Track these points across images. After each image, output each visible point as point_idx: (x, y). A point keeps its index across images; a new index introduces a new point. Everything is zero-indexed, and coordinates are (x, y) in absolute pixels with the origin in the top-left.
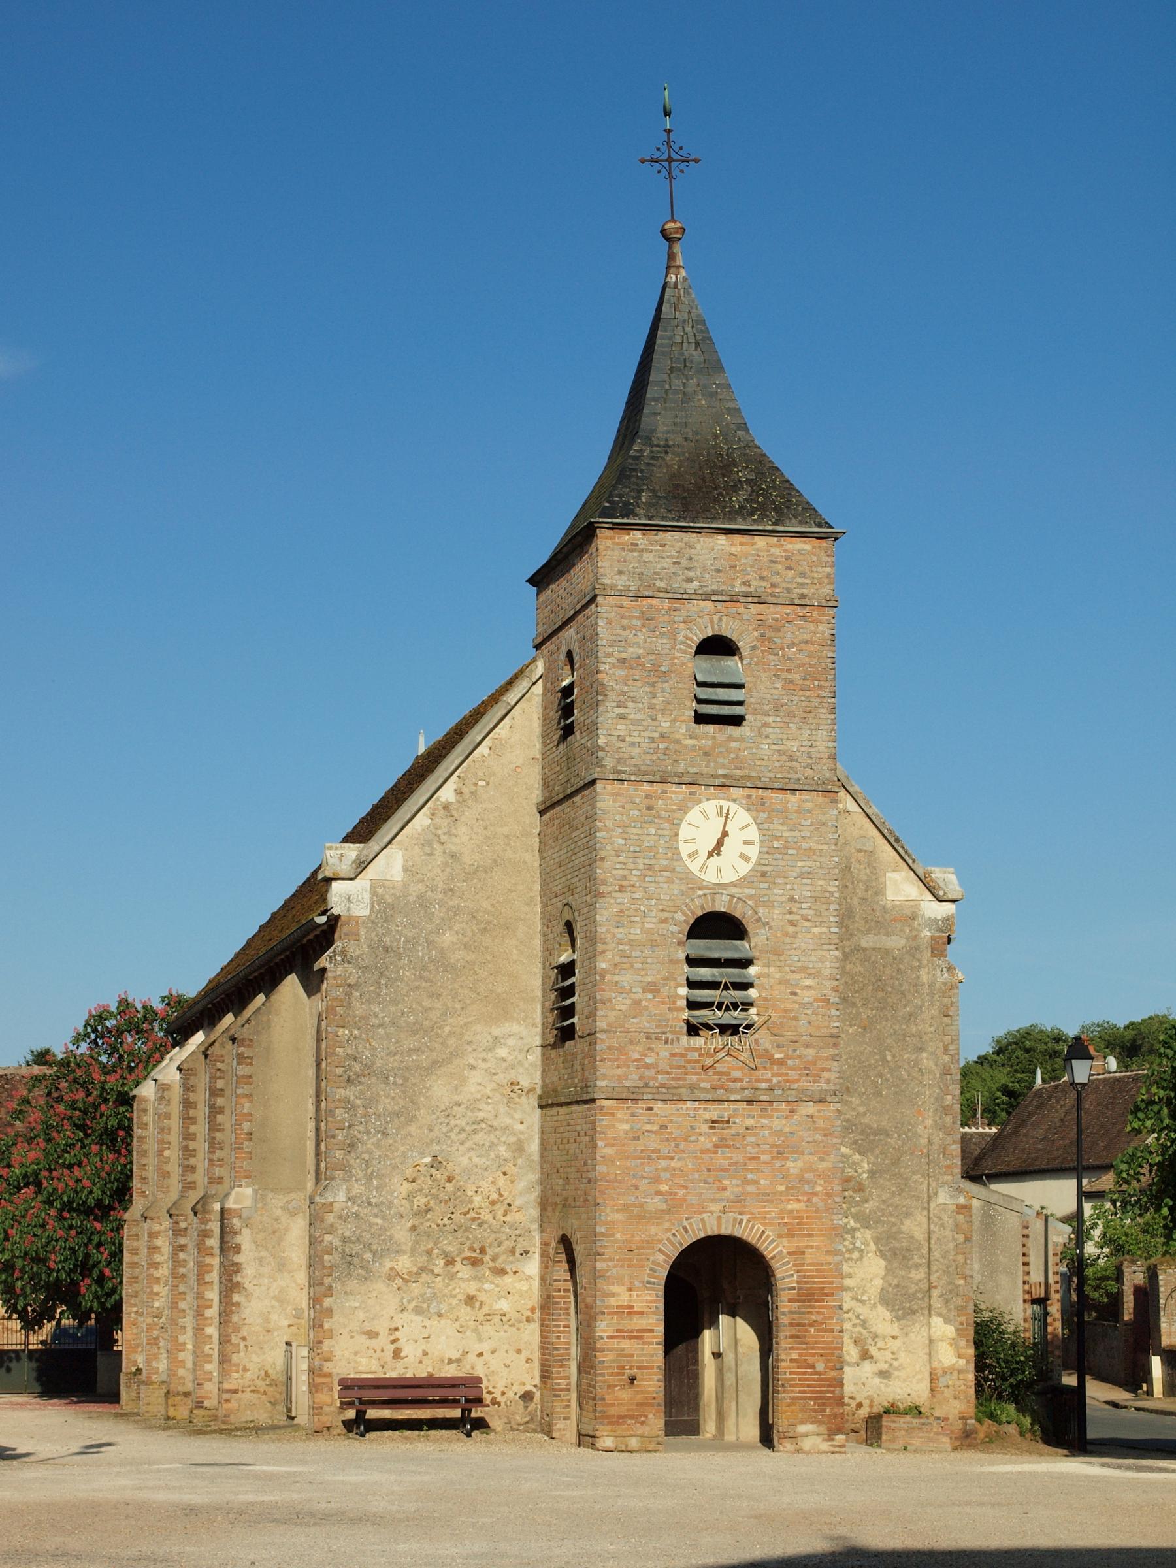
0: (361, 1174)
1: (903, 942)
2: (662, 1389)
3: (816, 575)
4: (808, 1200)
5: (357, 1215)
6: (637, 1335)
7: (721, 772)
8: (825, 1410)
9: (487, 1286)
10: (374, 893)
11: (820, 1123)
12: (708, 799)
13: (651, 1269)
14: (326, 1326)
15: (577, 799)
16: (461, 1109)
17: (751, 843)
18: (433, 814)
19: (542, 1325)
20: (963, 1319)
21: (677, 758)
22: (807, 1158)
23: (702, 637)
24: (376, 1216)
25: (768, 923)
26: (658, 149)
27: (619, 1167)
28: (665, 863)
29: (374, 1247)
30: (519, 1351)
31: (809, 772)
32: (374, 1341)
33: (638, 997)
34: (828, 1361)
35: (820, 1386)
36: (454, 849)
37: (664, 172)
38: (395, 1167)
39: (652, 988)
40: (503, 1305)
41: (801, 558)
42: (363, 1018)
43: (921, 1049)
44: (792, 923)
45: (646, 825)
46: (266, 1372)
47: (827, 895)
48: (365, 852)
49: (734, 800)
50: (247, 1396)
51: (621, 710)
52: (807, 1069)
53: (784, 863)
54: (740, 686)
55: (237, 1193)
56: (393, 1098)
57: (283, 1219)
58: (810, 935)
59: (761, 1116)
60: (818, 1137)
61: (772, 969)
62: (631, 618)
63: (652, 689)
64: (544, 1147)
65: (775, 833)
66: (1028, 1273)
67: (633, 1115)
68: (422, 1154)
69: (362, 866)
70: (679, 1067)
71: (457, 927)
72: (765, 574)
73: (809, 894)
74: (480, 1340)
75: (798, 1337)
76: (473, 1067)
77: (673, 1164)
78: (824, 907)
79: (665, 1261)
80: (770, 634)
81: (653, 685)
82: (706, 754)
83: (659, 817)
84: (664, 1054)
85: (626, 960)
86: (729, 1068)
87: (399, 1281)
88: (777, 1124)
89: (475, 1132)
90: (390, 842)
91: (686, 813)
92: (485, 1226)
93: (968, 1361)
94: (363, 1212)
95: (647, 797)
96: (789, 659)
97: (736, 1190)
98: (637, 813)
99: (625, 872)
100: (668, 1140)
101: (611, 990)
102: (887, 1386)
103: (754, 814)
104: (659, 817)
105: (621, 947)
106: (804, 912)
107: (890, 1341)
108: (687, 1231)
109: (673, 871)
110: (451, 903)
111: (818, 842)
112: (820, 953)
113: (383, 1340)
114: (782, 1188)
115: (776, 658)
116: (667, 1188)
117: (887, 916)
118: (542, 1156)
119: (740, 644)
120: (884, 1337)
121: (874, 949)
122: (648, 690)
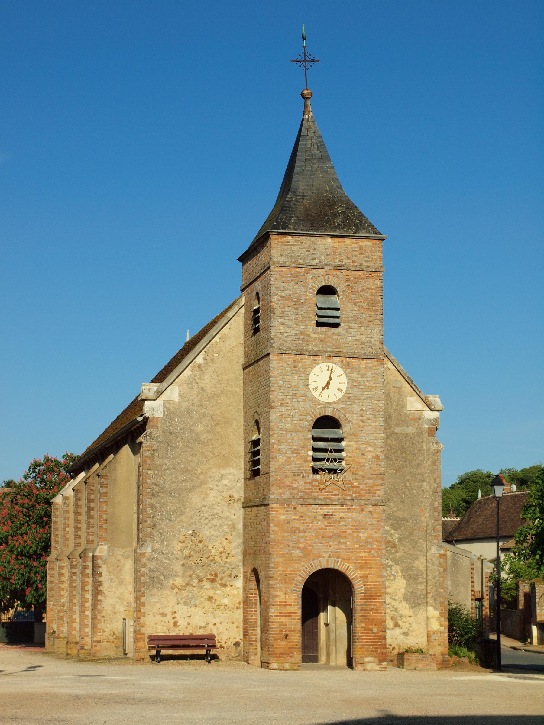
0: (159, 539)
1: (415, 430)
2: (301, 641)
3: (374, 257)
4: (370, 552)
6: (289, 615)
7: (329, 350)
8: (377, 651)
9: (218, 592)
10: (165, 407)
11: (375, 515)
12: (323, 363)
13: (295, 584)
15: (261, 362)
16: (206, 509)
17: (343, 383)
20: (443, 608)
21: (308, 343)
24: (166, 559)
25: (351, 421)
28: (303, 393)
29: (165, 573)
30: (233, 623)
31: (370, 350)
32: (164, 618)
33: (289, 456)
34: (379, 627)
35: (375, 639)
36: (203, 386)
37: (303, 67)
38: (174, 536)
39: (296, 452)
40: (226, 601)
41: (367, 249)
42: (160, 465)
43: (423, 481)
44: (362, 421)
46: (114, 633)
47: (379, 408)
49: (335, 363)
51: (281, 320)
53: (359, 393)
54: (338, 309)
55: (100, 548)
56: (174, 503)
58: (370, 427)
60: (374, 522)
61: (353, 443)
62: (286, 277)
63: (296, 311)
64: (245, 526)
65: (354, 379)
66: (474, 586)
68: (188, 530)
70: (309, 489)
71: (204, 423)
72: (350, 256)
73: (370, 407)
74: (215, 617)
75: (365, 616)
76: (211, 489)
77: (306, 534)
78: (378, 413)
79: (302, 580)
81: (297, 309)
83: (299, 371)
84: (302, 483)
86: (332, 489)
87: (176, 590)
88: (355, 516)
89: (212, 519)
90: (172, 383)
91: (312, 369)
92: (217, 564)
93: (445, 628)
94: (160, 557)
95: (294, 361)
96: (361, 296)
98: (289, 369)
99: (283, 397)
100: (303, 523)
101: (277, 453)
102: (407, 639)
103: (345, 369)
104: (299, 371)
105: (281, 432)
106: (368, 416)
107: (408, 618)
108: (312, 566)
110: (201, 411)
111: (374, 383)
112: (375, 435)
113: (169, 617)
114: (357, 546)
115: (355, 296)
116: (303, 546)
117: (407, 418)
119: (338, 289)
120: (405, 616)
121: (401, 433)
122: (294, 311)
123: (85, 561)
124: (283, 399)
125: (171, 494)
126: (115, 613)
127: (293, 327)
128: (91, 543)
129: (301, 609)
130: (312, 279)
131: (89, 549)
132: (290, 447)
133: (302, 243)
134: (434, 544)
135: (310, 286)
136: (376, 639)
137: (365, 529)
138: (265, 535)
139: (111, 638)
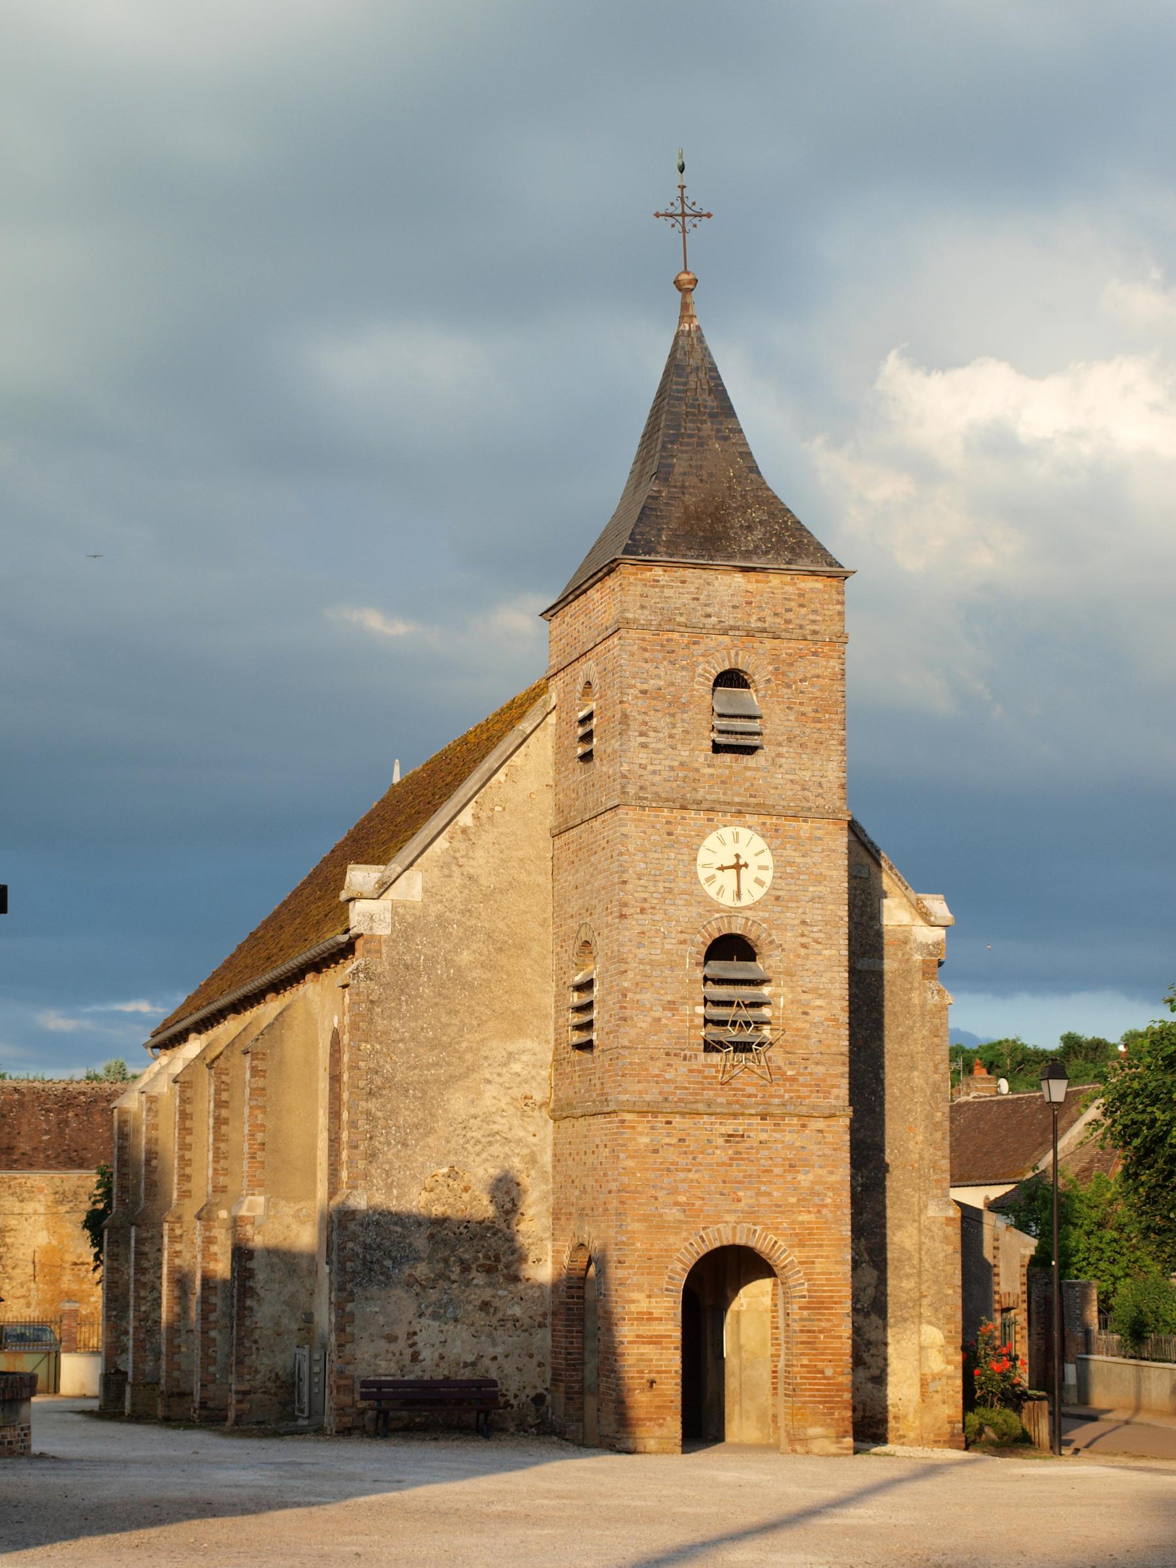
2: (679, 1393)
3: (827, 612)
4: (819, 1212)
5: (378, 1223)
6: (655, 1340)
7: (737, 799)
8: (833, 1414)
9: (500, 1292)
10: (394, 912)
11: (830, 1138)
13: (670, 1277)
14: (348, 1329)
15: (596, 824)
16: (477, 1122)
17: (766, 868)
18: (452, 838)
19: (554, 1330)
20: (952, 1327)
22: (820, 1172)
23: (720, 670)
26: (672, 204)
27: (640, 1179)
29: (394, 1254)
30: (531, 1356)
31: (820, 801)
32: (393, 1345)
33: (657, 1015)
34: (837, 1366)
35: (829, 1390)
36: (472, 871)
37: (678, 227)
39: (671, 1006)
40: (517, 1311)
41: (814, 595)
43: (913, 1068)
44: (804, 946)
45: (666, 850)
46: (277, 1374)
48: (387, 873)
49: (750, 827)
50: (259, 1396)
51: (643, 739)
52: (818, 1085)
53: (797, 888)
55: (251, 1201)
56: (413, 1111)
57: (294, 1227)
58: (820, 958)
59: (774, 1131)
60: (828, 1151)
62: (653, 650)
64: (557, 1158)
65: (789, 859)
67: (653, 1128)
68: (440, 1164)
69: (384, 887)
70: (697, 1083)
71: (475, 946)
72: (779, 611)
73: (820, 918)
74: (494, 1344)
75: (808, 1343)
76: (489, 1082)
77: (690, 1175)
78: (834, 930)
80: (783, 668)
81: (673, 715)
82: (723, 782)
83: (678, 842)
85: (647, 979)
86: (743, 1084)
87: (417, 1288)
88: (788, 1138)
89: (490, 1143)
90: (411, 864)
91: (704, 839)
92: (500, 1235)
93: (956, 1368)
96: (802, 692)
97: (750, 1201)
98: (657, 837)
99: (646, 895)
100: (686, 1153)
101: (632, 1008)
103: (768, 840)
106: (816, 935)
108: (703, 1241)
109: (691, 894)
110: (468, 923)
111: (829, 868)
112: (829, 975)
113: (402, 1343)
114: (793, 1200)
115: (789, 691)
116: (684, 1199)
118: (554, 1167)
121: (867, 972)
122: (668, 720)
123: (208, 1228)
124: (645, 900)
125: (407, 1091)
126: (279, 1335)
127: (666, 752)
128: (223, 1192)
129: (679, 1329)
130: (703, 655)
131: (217, 1204)
132: (664, 1000)
133: (683, 582)
134: (934, 1197)
135: (699, 670)
136: (832, 1390)
137: (808, 1165)
138: (605, 1175)
139: (269, 1384)
